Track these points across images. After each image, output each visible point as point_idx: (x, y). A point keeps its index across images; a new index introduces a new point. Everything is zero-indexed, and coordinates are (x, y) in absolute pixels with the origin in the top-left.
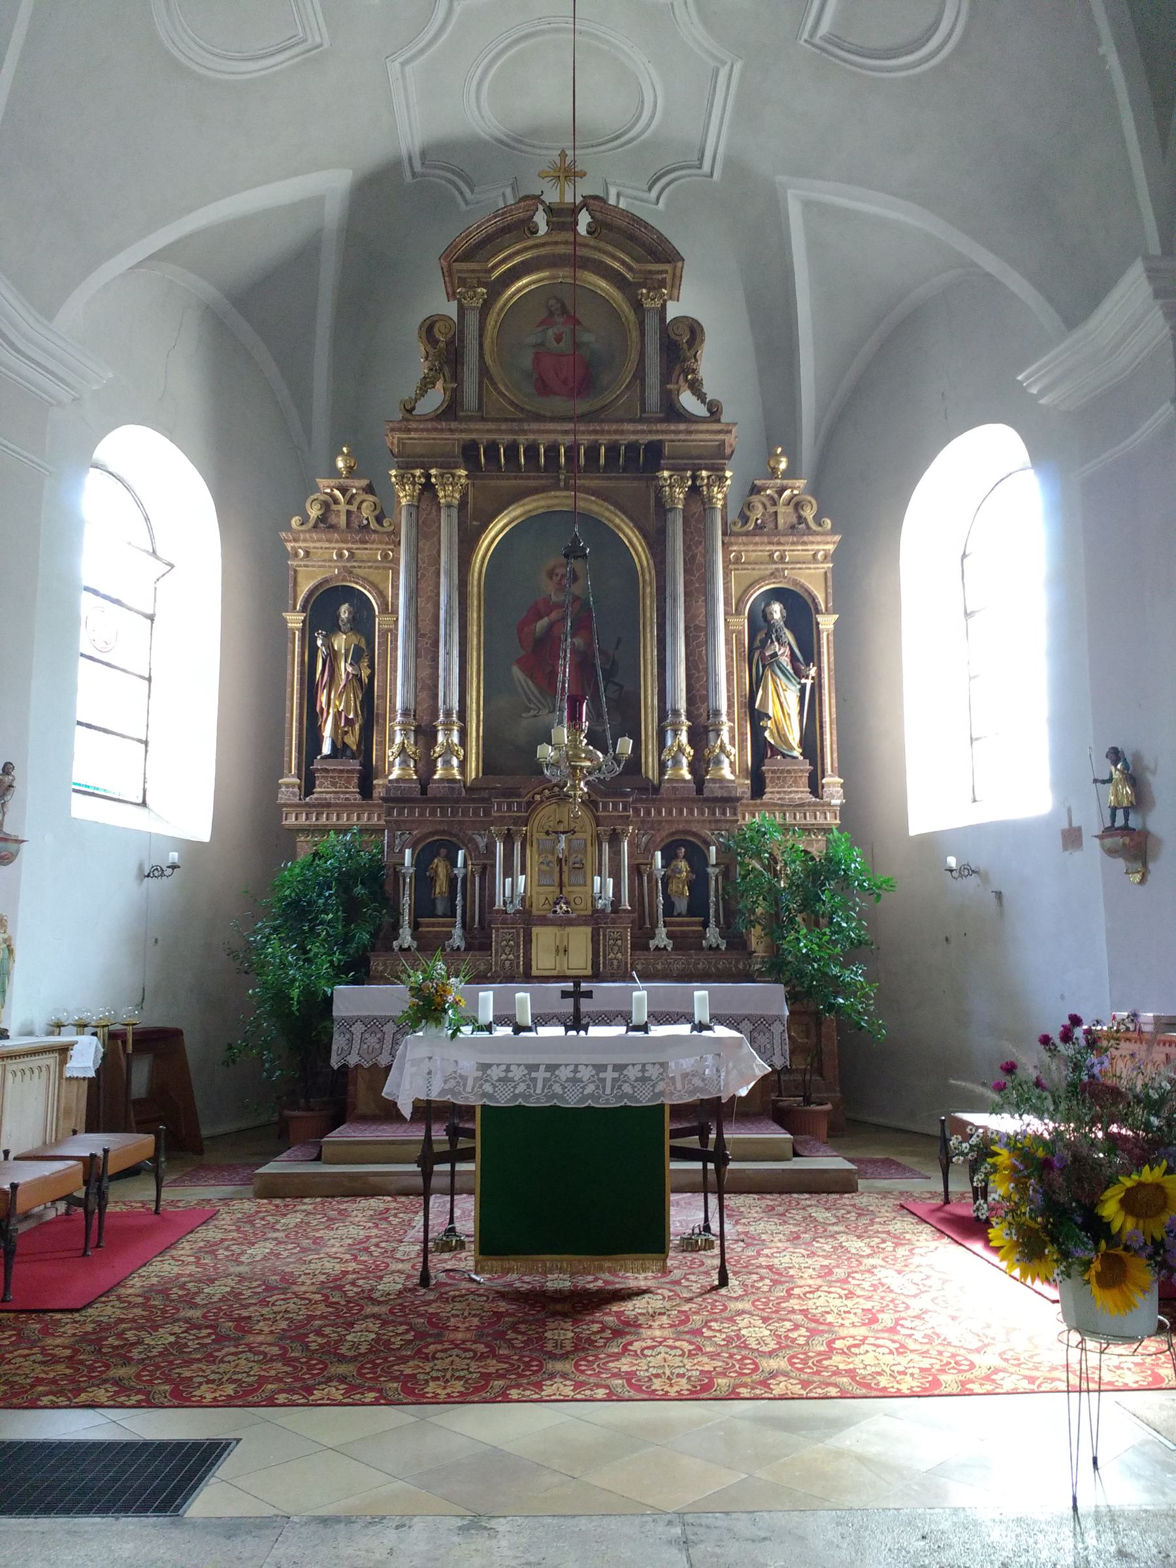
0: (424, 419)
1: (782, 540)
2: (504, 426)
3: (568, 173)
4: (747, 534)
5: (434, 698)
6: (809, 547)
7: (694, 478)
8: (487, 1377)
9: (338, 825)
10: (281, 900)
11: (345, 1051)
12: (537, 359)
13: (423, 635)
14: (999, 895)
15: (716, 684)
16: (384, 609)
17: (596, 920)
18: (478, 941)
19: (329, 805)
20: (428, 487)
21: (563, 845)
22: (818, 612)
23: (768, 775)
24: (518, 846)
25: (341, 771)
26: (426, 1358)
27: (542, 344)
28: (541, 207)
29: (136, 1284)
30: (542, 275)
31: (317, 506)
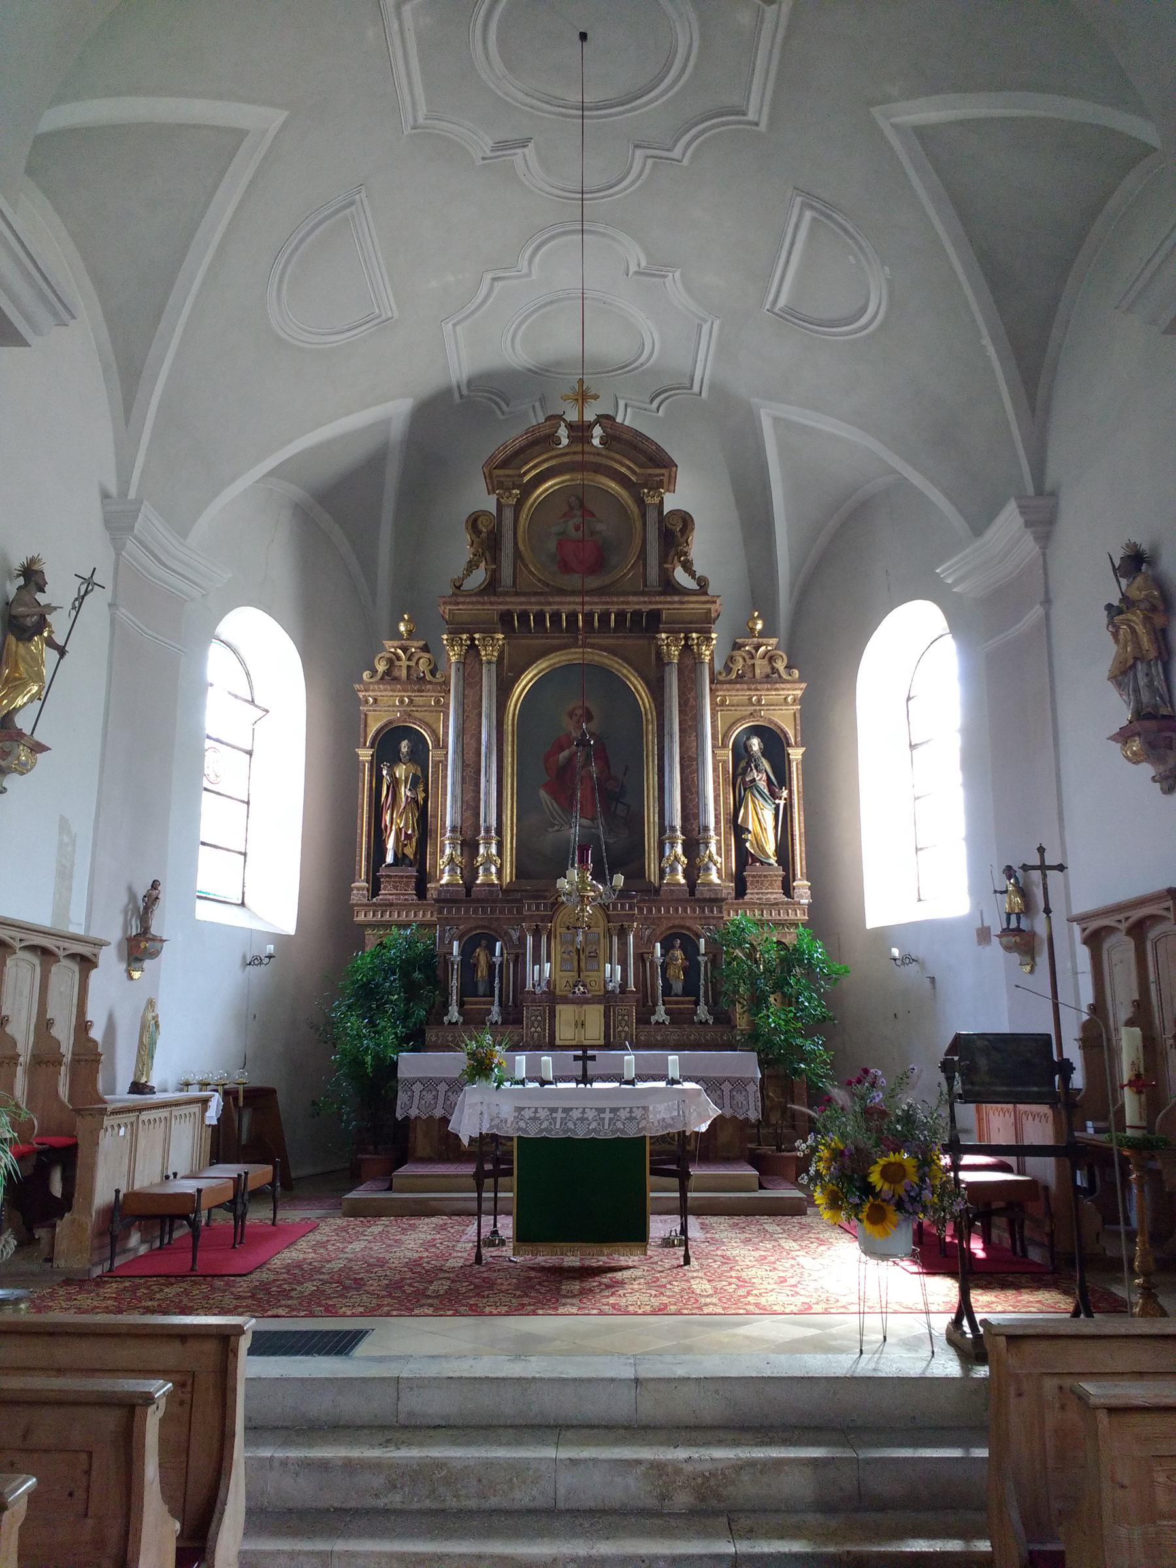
0: (470, 594)
1: (759, 687)
2: (533, 599)
3: (583, 397)
4: (730, 682)
5: (477, 815)
6: (781, 692)
7: (686, 638)
8: (523, 1305)
9: (396, 923)
10: (354, 983)
11: (407, 1105)
12: (560, 545)
13: (468, 766)
14: (933, 979)
15: (705, 805)
16: (437, 745)
17: (608, 999)
18: (512, 1017)
19: (391, 905)
20: (473, 646)
21: (580, 938)
22: (789, 745)
23: (749, 879)
24: (544, 939)
25: (402, 877)
26: (483, 1297)
27: (564, 532)
28: (563, 424)
29: (277, 1262)
30: (563, 478)
31: (383, 663)
